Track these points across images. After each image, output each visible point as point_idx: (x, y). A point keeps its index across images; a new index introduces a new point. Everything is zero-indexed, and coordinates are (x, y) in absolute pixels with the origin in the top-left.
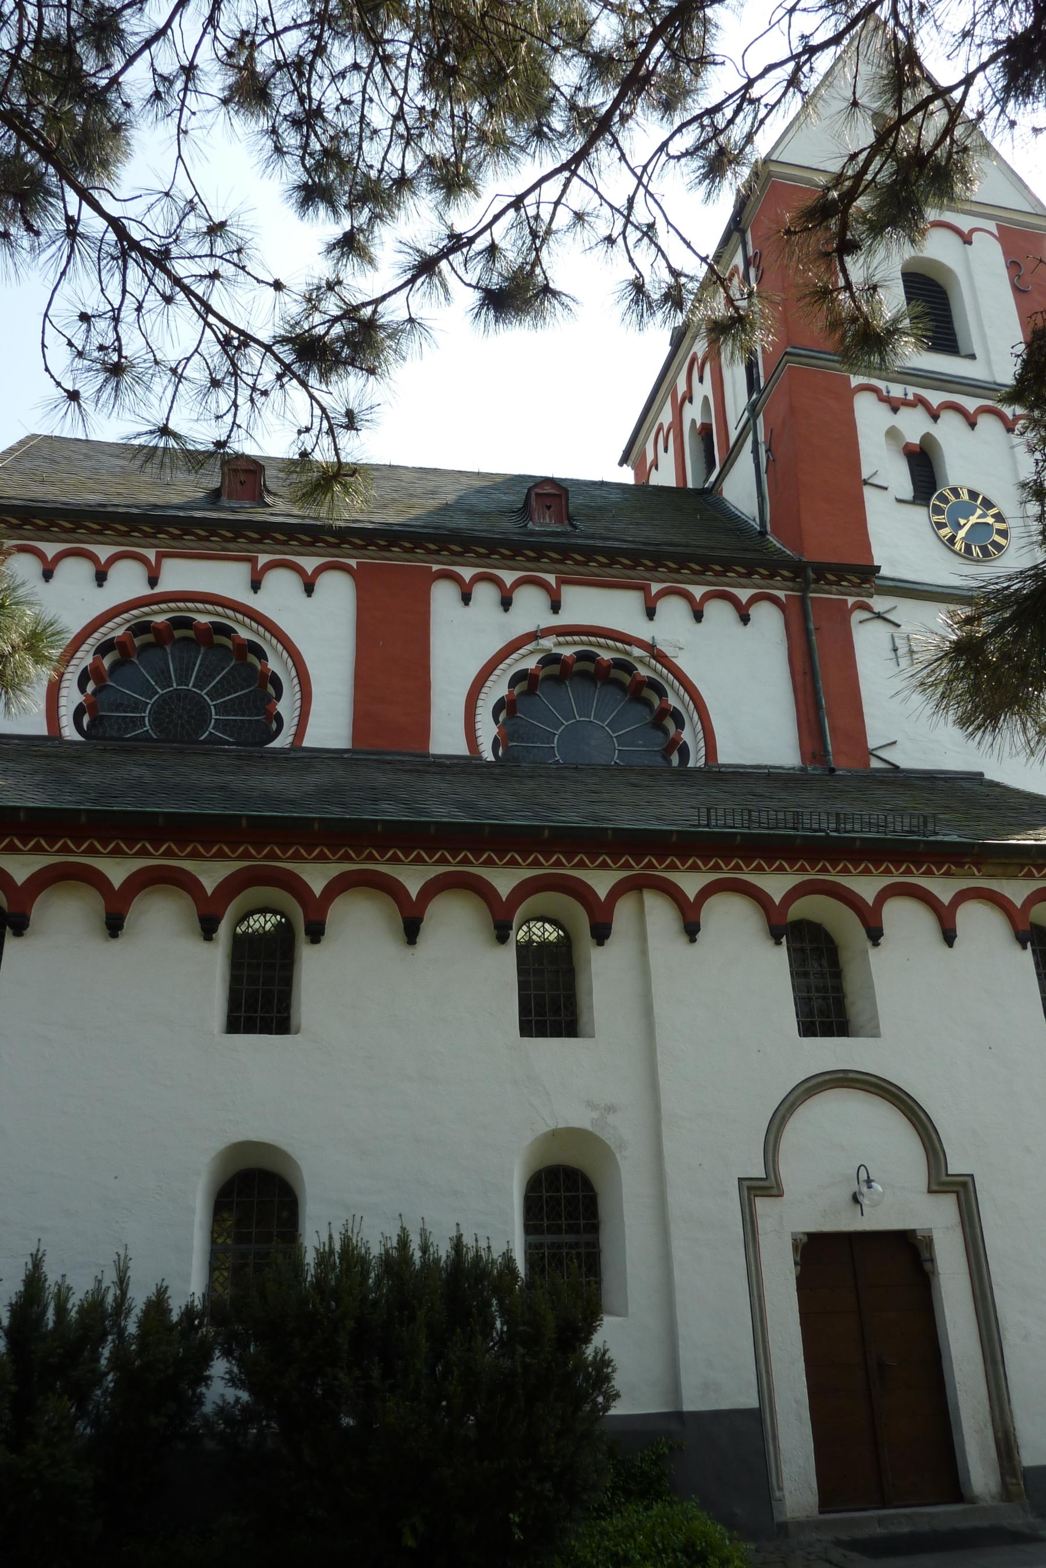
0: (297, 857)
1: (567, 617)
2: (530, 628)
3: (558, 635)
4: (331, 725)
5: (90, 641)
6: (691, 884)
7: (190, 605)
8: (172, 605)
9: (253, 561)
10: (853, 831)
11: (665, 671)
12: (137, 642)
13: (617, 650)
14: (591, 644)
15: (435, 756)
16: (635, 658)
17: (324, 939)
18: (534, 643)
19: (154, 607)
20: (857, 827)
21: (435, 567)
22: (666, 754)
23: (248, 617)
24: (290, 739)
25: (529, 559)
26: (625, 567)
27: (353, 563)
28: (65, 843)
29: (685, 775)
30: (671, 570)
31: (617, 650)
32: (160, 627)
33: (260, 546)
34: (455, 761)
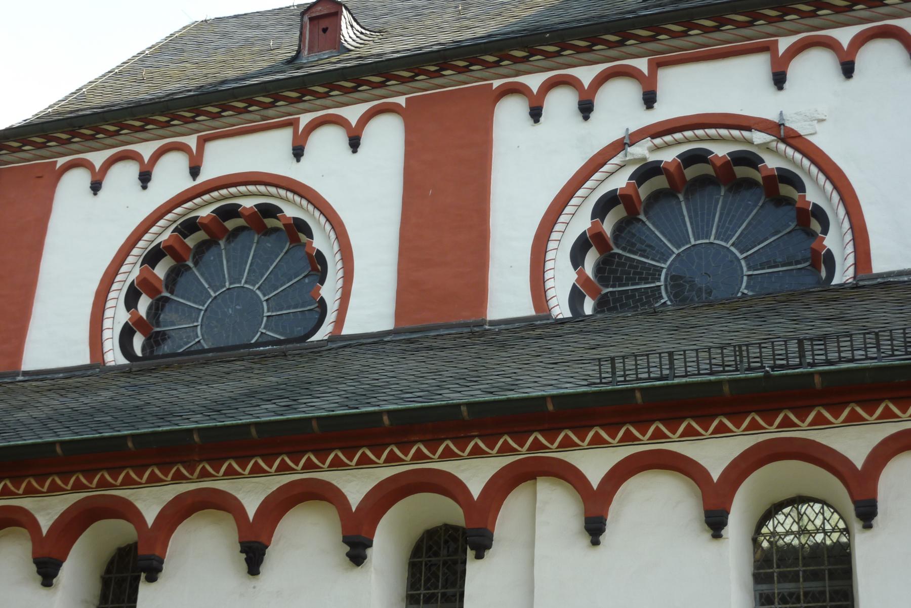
0: (128, 483)
1: (668, 109)
2: (617, 134)
3: (653, 137)
4: (369, 303)
5: (135, 251)
6: (595, 464)
7: (233, 190)
8: (215, 194)
9: (293, 124)
10: (841, 360)
11: (798, 156)
12: (191, 242)
13: (734, 140)
14: (699, 139)
15: (493, 323)
16: (759, 146)
17: (162, 577)
18: (621, 155)
19: (198, 201)
20: (859, 354)
21: (496, 83)
22: (815, 266)
23: (291, 191)
24: (851, 272)
25: (611, 45)
26: (739, 25)
27: (401, 100)
28: (786, 417)
29: (830, 294)
30: (803, 15)
31: (734, 140)
32: (206, 221)
33: (301, 106)
34: (517, 325)
